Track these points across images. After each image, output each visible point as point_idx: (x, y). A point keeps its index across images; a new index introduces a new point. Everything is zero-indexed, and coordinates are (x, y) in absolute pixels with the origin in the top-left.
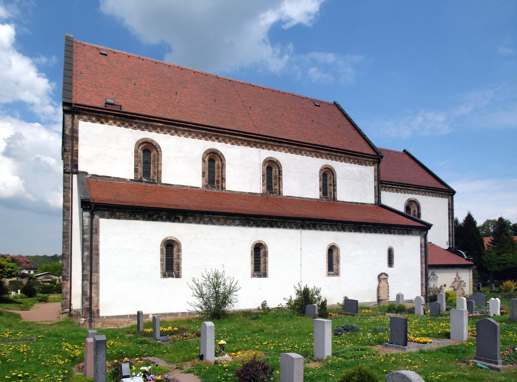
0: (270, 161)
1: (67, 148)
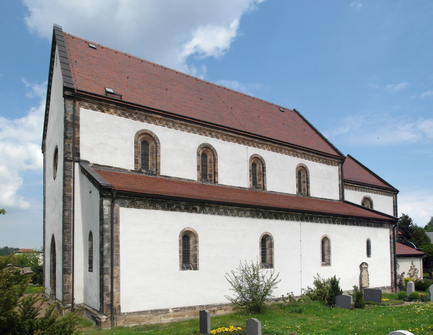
0: (255, 158)
1: (68, 135)
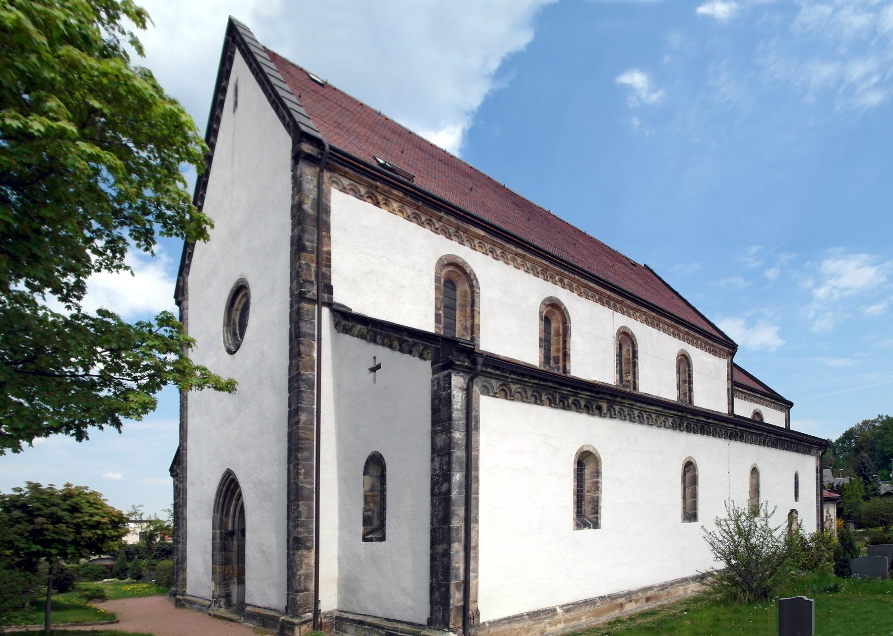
1: (308, 244)
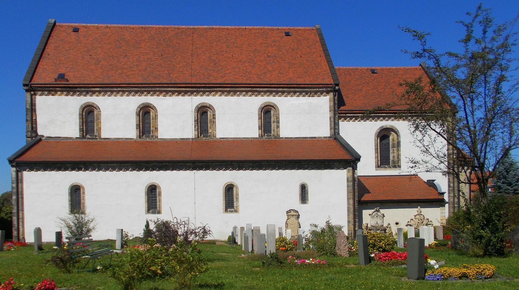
0: (141, 109)
